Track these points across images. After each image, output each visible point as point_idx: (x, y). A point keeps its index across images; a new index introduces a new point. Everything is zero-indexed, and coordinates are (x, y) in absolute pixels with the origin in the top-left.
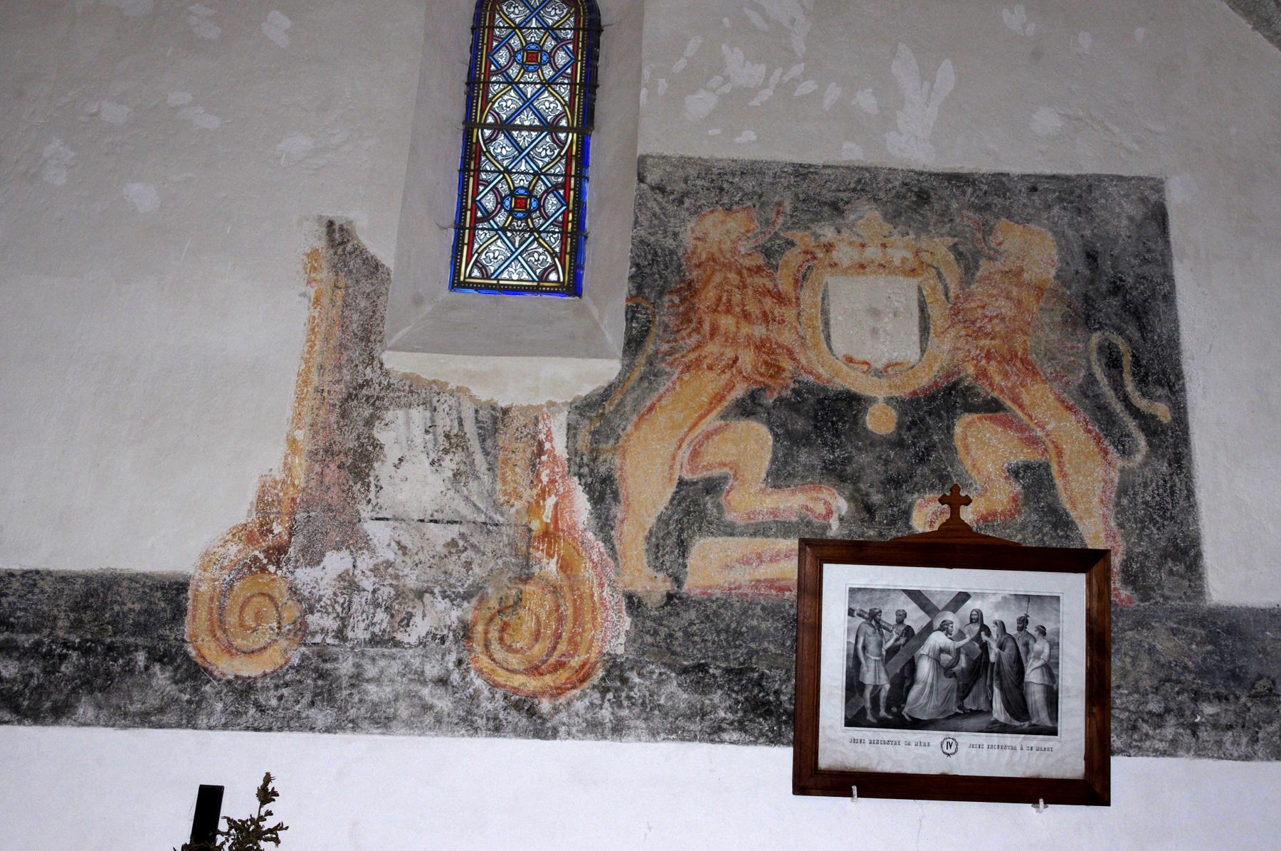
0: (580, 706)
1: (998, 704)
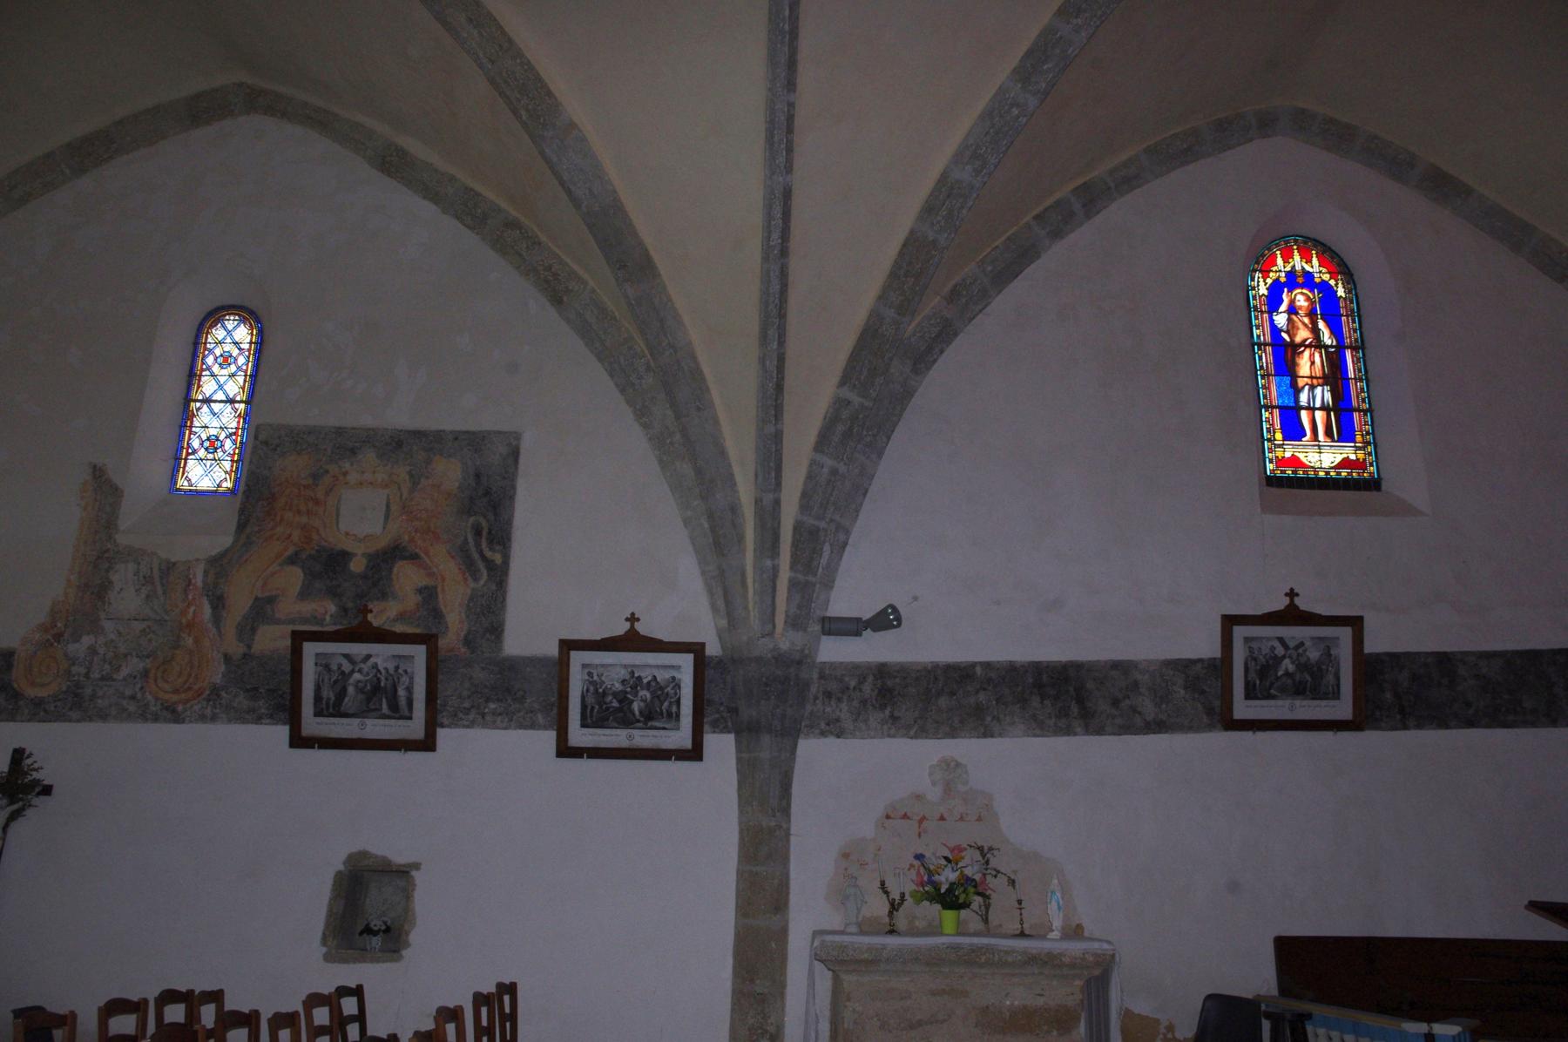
0: (196, 708)
1: (385, 706)
